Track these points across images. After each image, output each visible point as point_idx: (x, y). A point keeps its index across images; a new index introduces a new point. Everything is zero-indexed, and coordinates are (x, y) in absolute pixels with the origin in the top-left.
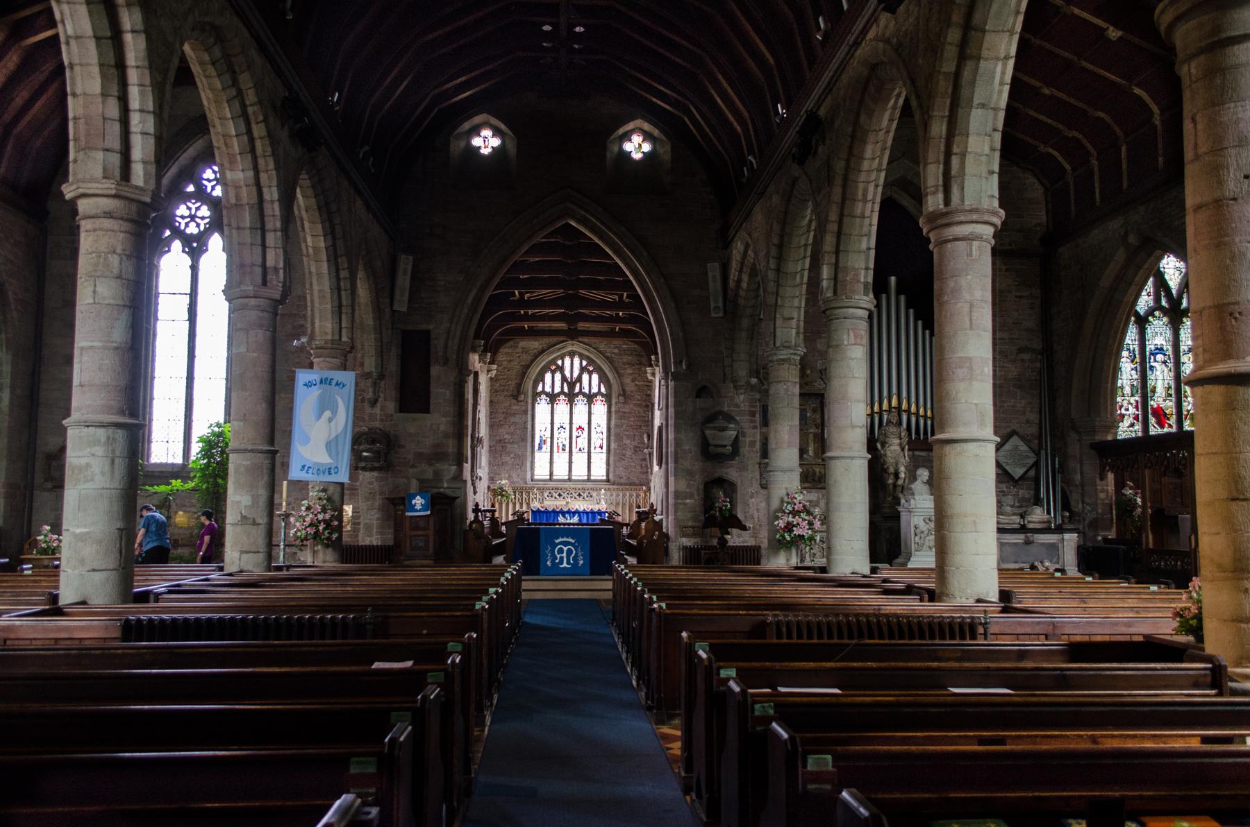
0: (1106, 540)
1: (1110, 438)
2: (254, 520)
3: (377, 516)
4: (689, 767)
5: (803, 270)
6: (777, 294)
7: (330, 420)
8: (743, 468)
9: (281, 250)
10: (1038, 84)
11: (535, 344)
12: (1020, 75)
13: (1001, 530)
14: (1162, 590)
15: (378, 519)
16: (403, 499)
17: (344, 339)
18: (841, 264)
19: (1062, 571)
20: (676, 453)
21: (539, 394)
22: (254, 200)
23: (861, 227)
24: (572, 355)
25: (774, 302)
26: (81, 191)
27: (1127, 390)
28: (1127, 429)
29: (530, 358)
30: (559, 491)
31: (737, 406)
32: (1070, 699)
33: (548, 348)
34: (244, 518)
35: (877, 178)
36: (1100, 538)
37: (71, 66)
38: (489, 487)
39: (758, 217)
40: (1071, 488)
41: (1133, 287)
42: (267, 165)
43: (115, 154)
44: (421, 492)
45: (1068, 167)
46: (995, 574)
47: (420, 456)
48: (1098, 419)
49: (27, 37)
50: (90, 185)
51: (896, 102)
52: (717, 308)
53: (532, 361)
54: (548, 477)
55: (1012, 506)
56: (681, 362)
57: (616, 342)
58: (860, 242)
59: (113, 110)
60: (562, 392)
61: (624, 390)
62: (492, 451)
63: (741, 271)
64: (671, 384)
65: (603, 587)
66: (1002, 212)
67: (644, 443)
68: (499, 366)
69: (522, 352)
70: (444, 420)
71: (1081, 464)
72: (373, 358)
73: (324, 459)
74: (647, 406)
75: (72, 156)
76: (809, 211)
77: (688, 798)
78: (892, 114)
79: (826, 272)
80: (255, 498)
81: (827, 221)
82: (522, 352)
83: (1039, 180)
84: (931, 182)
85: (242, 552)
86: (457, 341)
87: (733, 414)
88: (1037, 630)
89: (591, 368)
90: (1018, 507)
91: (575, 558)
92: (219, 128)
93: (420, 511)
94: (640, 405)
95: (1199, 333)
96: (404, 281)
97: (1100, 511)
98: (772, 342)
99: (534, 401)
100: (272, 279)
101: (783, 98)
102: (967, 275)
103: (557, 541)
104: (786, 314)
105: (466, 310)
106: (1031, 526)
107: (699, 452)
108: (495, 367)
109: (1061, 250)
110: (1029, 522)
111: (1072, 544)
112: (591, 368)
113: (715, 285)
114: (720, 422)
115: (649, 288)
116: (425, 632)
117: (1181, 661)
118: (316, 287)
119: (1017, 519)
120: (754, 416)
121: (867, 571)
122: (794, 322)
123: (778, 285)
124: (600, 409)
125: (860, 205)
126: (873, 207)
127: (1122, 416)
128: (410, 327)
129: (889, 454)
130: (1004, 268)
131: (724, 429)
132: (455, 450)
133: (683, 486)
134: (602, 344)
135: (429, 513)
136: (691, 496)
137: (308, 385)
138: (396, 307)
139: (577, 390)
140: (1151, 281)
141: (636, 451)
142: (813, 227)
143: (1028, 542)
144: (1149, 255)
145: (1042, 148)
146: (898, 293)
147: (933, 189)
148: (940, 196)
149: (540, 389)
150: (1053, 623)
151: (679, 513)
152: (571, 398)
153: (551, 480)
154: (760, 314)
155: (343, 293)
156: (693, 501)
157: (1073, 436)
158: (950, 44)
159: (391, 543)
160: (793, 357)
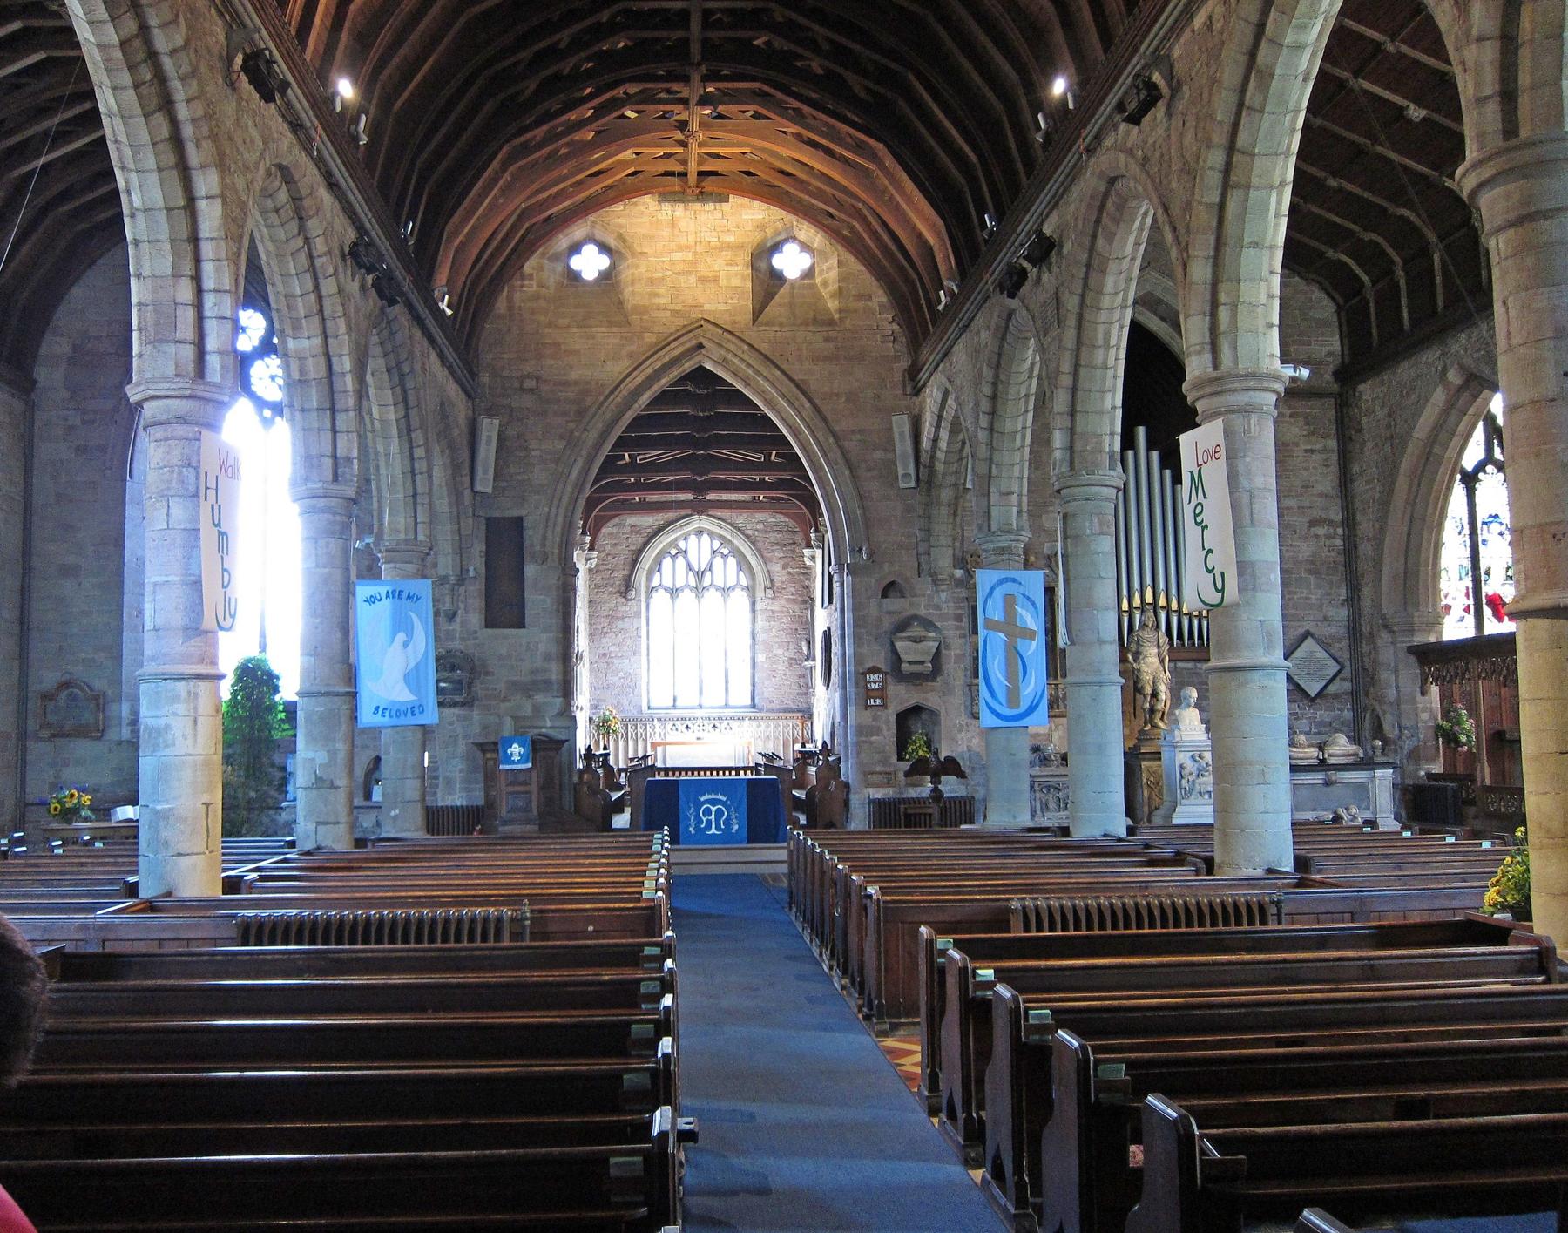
0: (1430, 776)
1: (1432, 639)
2: (332, 782)
3: (460, 767)
4: (933, 1084)
5: (1024, 428)
6: (991, 460)
7: (406, 645)
8: (947, 691)
9: (355, 435)
10: (1321, 174)
11: (649, 521)
12: (1305, 167)
13: (1295, 769)
14: (1497, 848)
15: (461, 771)
16: (496, 744)
17: (421, 537)
18: (1078, 429)
19: (1372, 823)
22: (323, 373)
23: (1104, 379)
25: (987, 472)
26: (151, 393)
27: (1454, 574)
28: (1456, 628)
29: (641, 540)
30: (687, 722)
31: (938, 607)
32: (1377, 994)
33: (667, 526)
34: (319, 780)
35: (1122, 317)
36: (1422, 773)
37: (136, 242)
38: (590, 719)
39: (960, 354)
40: (1384, 707)
41: (1456, 439)
42: (338, 328)
43: (188, 346)
44: (517, 737)
45: (1365, 278)
46: (1290, 834)
47: (515, 686)
48: (1416, 614)
49: (15, 168)
50: (161, 386)
51: (1142, 223)
52: (906, 475)
53: (645, 544)
55: (1307, 733)
56: (861, 549)
57: (761, 515)
58: (1102, 399)
59: (185, 292)
60: (687, 585)
61: (772, 581)
62: (594, 668)
63: (938, 427)
65: (774, 858)
67: (802, 653)
68: (600, 552)
69: (632, 532)
70: (544, 636)
71: (1396, 671)
72: (450, 558)
73: (404, 696)
74: (805, 602)
75: (136, 350)
76: (1030, 352)
77: (935, 1120)
78: (1139, 236)
79: (1058, 439)
80: (332, 753)
81: (1058, 373)
82: (632, 532)
83: (1328, 294)
85: (319, 823)
86: (559, 529)
87: (933, 619)
88: (1340, 907)
89: (726, 551)
90: (1315, 734)
91: (728, 822)
92: (280, 288)
93: (519, 762)
94: (795, 601)
95: (1518, 557)
96: (487, 452)
97: (1422, 737)
98: (986, 524)
100: (344, 473)
101: (991, 209)
102: (1245, 457)
103: (702, 799)
104: (1004, 488)
105: (569, 489)
106: (1332, 761)
108: (595, 554)
109: (1361, 387)
110: (1330, 756)
111: (1387, 783)
112: (726, 551)
113: (904, 446)
115: (815, 452)
116: (591, 928)
117: (1506, 944)
118: (383, 471)
119: (1314, 752)
120: (961, 621)
121: (1122, 832)
122: (1014, 498)
123: (991, 447)
125: (1101, 352)
126: (1117, 354)
127: (1448, 608)
128: (497, 514)
129: (1144, 668)
130: (1288, 413)
132: (561, 677)
134: (740, 519)
135: (530, 765)
137: (372, 600)
138: (479, 488)
140: (1480, 427)
141: (791, 665)
142: (1036, 372)
143: (1328, 783)
144: (1476, 397)
145: (1330, 253)
146: (1149, 448)
147: (1198, 347)
148: (1207, 357)
149: (655, 583)
150: (1360, 898)
151: (863, 755)
152: (699, 590)
153: (674, 707)
154: (964, 484)
155: (418, 478)
157: (1385, 637)
158: (1210, 168)
159: (481, 802)
160: (1013, 544)
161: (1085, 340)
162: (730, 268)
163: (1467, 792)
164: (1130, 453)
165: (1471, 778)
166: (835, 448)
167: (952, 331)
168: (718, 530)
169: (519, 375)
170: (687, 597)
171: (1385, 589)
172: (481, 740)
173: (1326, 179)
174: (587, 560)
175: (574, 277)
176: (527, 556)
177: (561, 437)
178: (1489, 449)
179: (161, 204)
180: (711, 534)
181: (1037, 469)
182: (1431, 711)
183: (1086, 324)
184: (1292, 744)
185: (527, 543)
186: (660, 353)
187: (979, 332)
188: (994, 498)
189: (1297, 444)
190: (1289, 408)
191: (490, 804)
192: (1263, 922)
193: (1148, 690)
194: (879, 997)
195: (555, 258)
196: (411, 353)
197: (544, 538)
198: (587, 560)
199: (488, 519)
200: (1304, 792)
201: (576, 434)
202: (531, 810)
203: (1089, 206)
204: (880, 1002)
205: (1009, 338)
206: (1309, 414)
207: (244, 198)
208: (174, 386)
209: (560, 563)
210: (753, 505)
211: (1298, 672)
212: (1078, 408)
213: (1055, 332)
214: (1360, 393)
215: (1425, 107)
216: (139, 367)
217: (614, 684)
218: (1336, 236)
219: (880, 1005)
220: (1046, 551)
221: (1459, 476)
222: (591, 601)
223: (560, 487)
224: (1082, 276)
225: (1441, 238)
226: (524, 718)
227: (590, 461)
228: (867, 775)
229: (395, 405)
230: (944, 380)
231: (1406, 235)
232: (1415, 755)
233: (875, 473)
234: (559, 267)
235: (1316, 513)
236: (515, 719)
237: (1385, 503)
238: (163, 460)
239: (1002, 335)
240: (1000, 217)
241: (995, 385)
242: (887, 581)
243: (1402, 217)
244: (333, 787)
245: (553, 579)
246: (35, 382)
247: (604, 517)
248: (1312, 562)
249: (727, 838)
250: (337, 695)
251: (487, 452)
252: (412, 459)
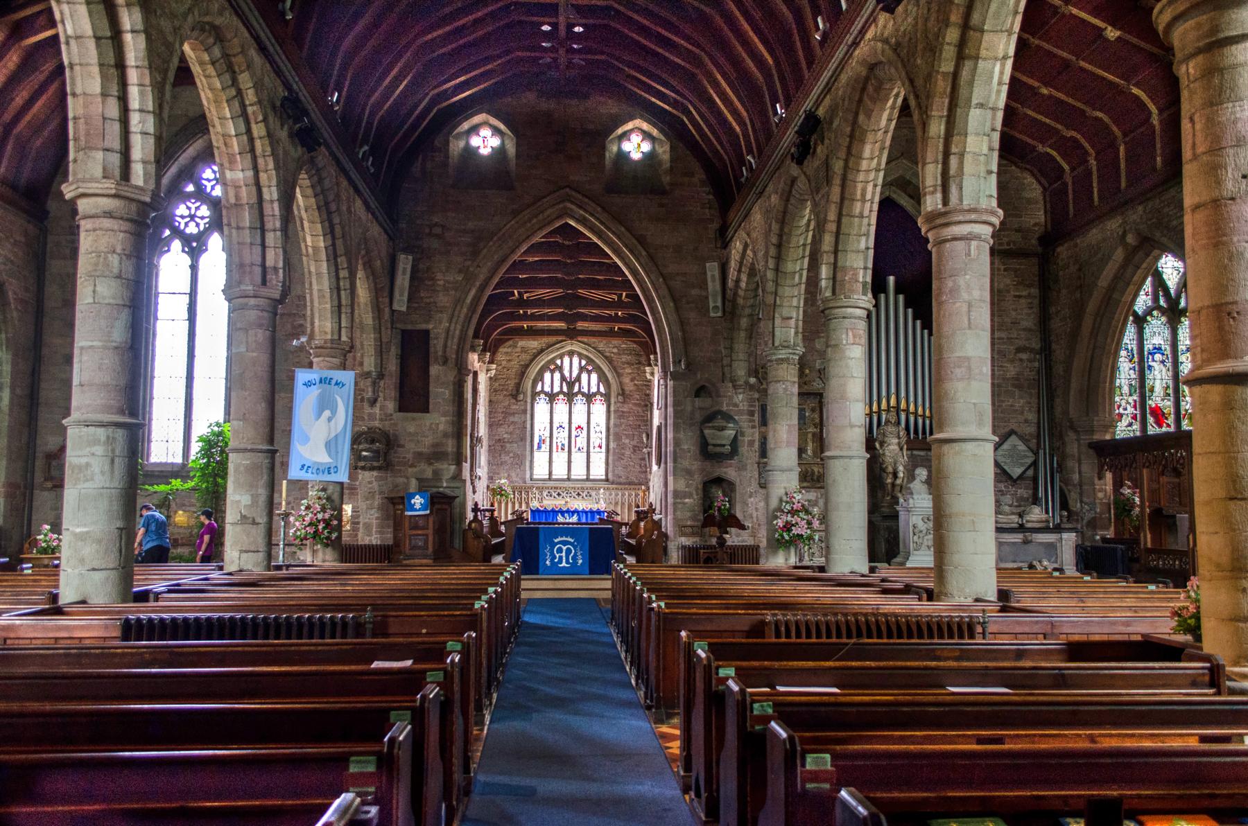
0: (1104, 540)
1: (1108, 437)
2: (254, 519)
4: (688, 767)
5: (801, 269)
6: (776, 294)
7: (330, 420)
8: (742, 468)
10: (1036, 84)
11: (534, 344)
13: (999, 530)
16: (402, 498)
17: (344, 338)
18: (839, 264)
19: (1061, 570)
22: (254, 200)
23: (860, 226)
24: (571, 354)
26: (81, 190)
28: (1125, 429)
29: (529, 357)
31: (736, 405)
34: (244, 517)
36: (1098, 537)
37: (71, 66)
38: (488, 487)
39: (757, 217)
41: (1131, 287)
42: (266, 165)
44: (421, 491)
45: (1066, 167)
47: (419, 455)
48: (1096, 418)
50: (90, 185)
52: (716, 307)
53: (532, 361)
56: (680, 361)
57: (616, 342)
58: (859, 242)
59: (113, 109)
60: (561, 392)
61: (623, 390)
63: (739, 271)
64: (670, 383)
65: (602, 587)
66: (1001, 212)
69: (522, 352)
70: (443, 419)
72: (373, 358)
73: (324, 458)
77: (687, 797)
79: (824, 272)
80: (254, 498)
81: (825, 220)
82: (522, 352)
84: (929, 181)
86: (456, 340)
87: (732, 413)
88: (1036, 629)
89: (590, 368)
91: (574, 558)
93: (419, 510)
94: (639, 405)
96: (403, 280)
97: (1098, 510)
98: (770, 342)
100: (271, 279)
103: (556, 541)
105: (465, 310)
106: (1029, 525)
108: (494, 366)
109: (1059, 249)
110: (1027, 521)
112: (590, 368)
113: (714, 286)
114: (719, 422)
116: (424, 631)
118: (315, 287)
119: (1015, 518)
120: (753, 415)
121: (865, 570)
122: (793, 322)
123: (777, 284)
124: (599, 409)
125: (858, 204)
127: (1121, 416)
128: (409, 327)
129: (887, 453)
131: (723, 429)
132: (455, 450)
133: (682, 485)
134: (602, 344)
135: (428, 512)
136: (690, 495)
137: (308, 384)
138: (396, 307)
139: (576, 389)
141: (635, 451)
142: (812, 227)
143: (1026, 542)
144: (1148, 255)
145: (1040, 148)
147: (931, 189)
148: (939, 196)
149: (539, 388)
150: (1052, 623)
151: (678, 513)
152: (570, 397)
153: (550, 479)
155: (343, 293)
157: (1071, 435)
158: (948, 44)
159: (391, 542)
161: (847, 195)
163: (1133, 553)
164: (882, 296)
165: (1137, 542)
166: (664, 286)
167: (752, 197)
171: (1072, 399)
172: (392, 495)
173: (1039, 87)
174: (488, 371)
176: (432, 360)
177: (460, 271)
178: (1156, 299)
179: (90, 32)
180: (581, 356)
181: (812, 305)
182: (1105, 491)
183: (849, 183)
184: (997, 512)
185: (432, 350)
187: (770, 196)
188: (778, 321)
189: (1008, 291)
190: (1004, 264)
191: (397, 543)
192: (972, 636)
193: (890, 469)
194: (658, 690)
196: (338, 196)
197: (445, 346)
198: (488, 371)
199: (404, 332)
200: (1006, 549)
201: (471, 269)
202: (427, 549)
203: (854, 89)
204: (659, 695)
205: (792, 201)
206: (1019, 269)
207: (171, 39)
208: (100, 186)
209: (456, 365)
210: (610, 334)
211: (1003, 460)
212: (840, 248)
213: (824, 190)
214: (1058, 254)
215: (1120, 29)
216: (74, 171)
217: (505, 462)
218: (1045, 134)
219: (658, 697)
220: (818, 366)
221: (1131, 318)
222: (490, 401)
223: (458, 308)
224: (846, 144)
225: (1125, 135)
226: (427, 480)
227: (482, 289)
228: (682, 529)
229: (324, 235)
230: (745, 235)
231: (1098, 132)
232: (1093, 524)
233: (693, 305)
235: (1021, 343)
236: (420, 480)
237: (1074, 335)
238: (91, 247)
239: (787, 197)
240: (786, 106)
241: (780, 236)
242: (698, 386)
243: (1096, 118)
244: (254, 523)
245: (451, 376)
246: (48, 212)
247: (501, 339)
248: (1017, 379)
249: (573, 571)
250: (261, 451)
251: (403, 280)
252: (338, 279)
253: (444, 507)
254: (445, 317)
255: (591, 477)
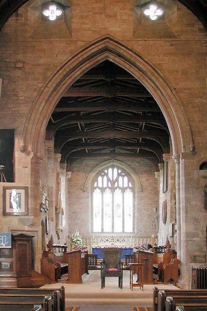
20: (186, 207)
21: (95, 188)
24: (113, 167)
38: (69, 236)
54: (101, 231)
60: (108, 187)
74: (155, 193)
89: (123, 174)
99: (92, 191)
107: (203, 206)
124: (129, 195)
133: (191, 229)
135: (10, 247)
136: (197, 235)
139: (116, 185)
149: (95, 185)
151: (189, 247)
152: (113, 189)
156: (199, 239)
162: (122, 11)
168: (120, 166)
169: (14, 61)
170: (108, 191)
175: (45, 19)
186: (86, 51)
195: (35, 8)
223: (34, 114)
234: (37, 14)
242: (201, 162)
253: (25, 243)
254: (24, 120)
255: (125, 231)
